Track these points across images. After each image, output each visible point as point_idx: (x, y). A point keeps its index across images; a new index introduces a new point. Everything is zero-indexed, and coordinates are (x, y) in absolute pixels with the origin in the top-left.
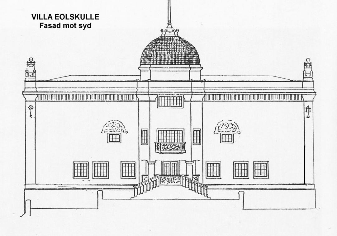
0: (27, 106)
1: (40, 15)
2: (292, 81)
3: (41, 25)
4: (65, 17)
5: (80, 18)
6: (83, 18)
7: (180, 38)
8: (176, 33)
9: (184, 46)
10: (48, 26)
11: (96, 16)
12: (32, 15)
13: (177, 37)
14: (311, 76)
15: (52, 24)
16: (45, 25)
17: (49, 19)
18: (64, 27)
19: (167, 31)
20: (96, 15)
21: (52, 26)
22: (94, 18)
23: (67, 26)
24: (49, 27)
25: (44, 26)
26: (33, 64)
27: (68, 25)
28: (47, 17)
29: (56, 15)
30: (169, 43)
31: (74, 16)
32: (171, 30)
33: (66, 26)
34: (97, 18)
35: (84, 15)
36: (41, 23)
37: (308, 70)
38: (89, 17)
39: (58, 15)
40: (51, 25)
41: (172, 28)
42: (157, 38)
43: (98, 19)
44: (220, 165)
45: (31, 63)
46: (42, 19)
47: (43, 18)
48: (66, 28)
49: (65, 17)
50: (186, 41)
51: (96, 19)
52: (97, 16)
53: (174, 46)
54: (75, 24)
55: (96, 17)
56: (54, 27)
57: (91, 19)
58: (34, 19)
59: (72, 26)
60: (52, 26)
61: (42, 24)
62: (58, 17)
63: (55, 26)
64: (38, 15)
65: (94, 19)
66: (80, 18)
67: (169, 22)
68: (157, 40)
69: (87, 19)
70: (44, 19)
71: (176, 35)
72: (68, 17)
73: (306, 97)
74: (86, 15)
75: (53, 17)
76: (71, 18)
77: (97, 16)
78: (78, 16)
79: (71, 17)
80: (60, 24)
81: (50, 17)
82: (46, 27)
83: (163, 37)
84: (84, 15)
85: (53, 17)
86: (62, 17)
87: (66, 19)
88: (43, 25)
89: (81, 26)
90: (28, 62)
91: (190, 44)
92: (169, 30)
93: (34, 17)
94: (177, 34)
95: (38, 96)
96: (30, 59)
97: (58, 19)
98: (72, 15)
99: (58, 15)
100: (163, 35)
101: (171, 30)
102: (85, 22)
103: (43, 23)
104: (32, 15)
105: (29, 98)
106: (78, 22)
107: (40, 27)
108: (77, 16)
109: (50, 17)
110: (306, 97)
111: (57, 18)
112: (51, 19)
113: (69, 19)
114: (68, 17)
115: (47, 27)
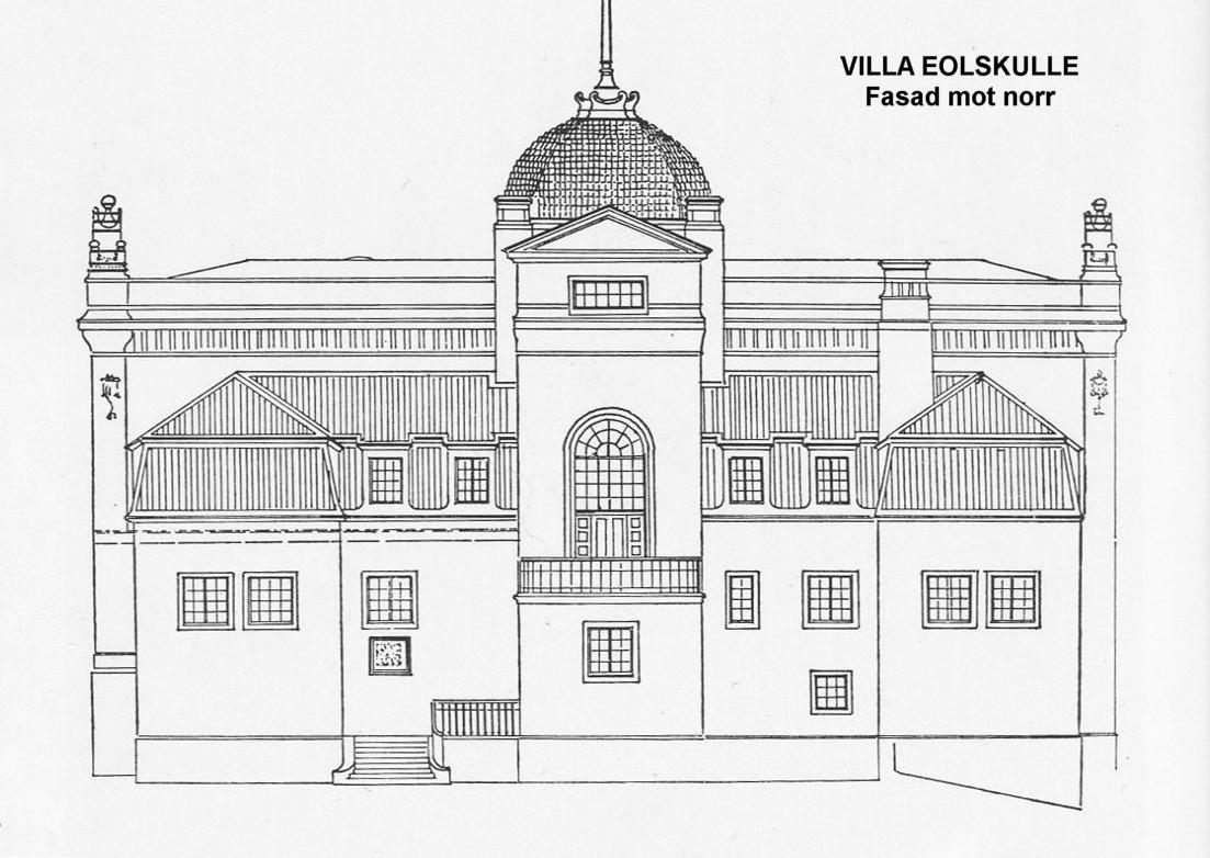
0: (100, 373)
1: (869, 58)
2: (1051, 281)
3: (869, 96)
4: (960, 66)
5: (1010, 69)
6: (1021, 68)
7: (644, 124)
8: (629, 106)
9: (658, 152)
10: (895, 99)
11: (1069, 64)
12: (843, 59)
13: (633, 123)
14: (1111, 263)
15: (910, 92)
16: (884, 94)
17: (903, 72)
18: (951, 103)
19: (596, 97)
20: (1066, 58)
21: (910, 97)
22: (1062, 70)
23: (964, 97)
24: (898, 103)
25: (881, 97)
26: (116, 217)
27: (967, 94)
28: (893, 66)
29: (925, 58)
30: (603, 141)
31: (991, 64)
32: (613, 94)
33: (957, 97)
34: (1070, 69)
35: (1026, 58)
36: (869, 89)
37: (1099, 240)
38: (1042, 66)
39: (935, 58)
40: (906, 94)
41: (615, 87)
42: (562, 125)
43: (1076, 74)
44: (414, 581)
45: (108, 214)
46: (1043, 74)
47: (1046, 70)
48: (959, 104)
49: (960, 66)
50: (665, 135)
51: (1066, 73)
52: (1070, 62)
53: (621, 154)
54: (991, 92)
55: (1066, 65)
56: (917, 101)
57: (1051, 73)
58: (849, 73)
59: (979, 98)
60: (910, 97)
61: (873, 92)
62: (934, 65)
63: (918, 99)
64: (862, 58)
65: (1059, 74)
66: (1010, 69)
67: (607, 68)
68: (560, 130)
69: (1035, 73)
70: (886, 73)
71: (631, 115)
72: (971, 66)
73: (1092, 342)
74: (1034, 58)
75: (917, 66)
76: (978, 71)
77: (1070, 62)
78: (1005, 64)
79: (979, 68)
80: (936, 92)
81: (906, 66)
82: (887, 101)
83: (582, 119)
84: (1026, 58)
85: (917, 66)
86: (948, 66)
87: (963, 73)
88: (876, 96)
89: (903, 98)
90: (96, 212)
91: (678, 145)
92: (603, 94)
93: (849, 66)
94: (634, 110)
95: (133, 335)
96: (105, 201)
97: (935, 74)
98: (983, 61)
99: (935, 58)
100: (583, 115)
101: (613, 94)
102: (1031, 83)
103: (877, 88)
104: (843, 59)
105: (102, 341)
106: (1001, 83)
107: (869, 103)
108: (999, 65)
109: (906, 66)
110: (1092, 342)
111: (929, 70)
112: (908, 72)
113: (972, 74)
114: (971, 66)
115: (921, 103)
